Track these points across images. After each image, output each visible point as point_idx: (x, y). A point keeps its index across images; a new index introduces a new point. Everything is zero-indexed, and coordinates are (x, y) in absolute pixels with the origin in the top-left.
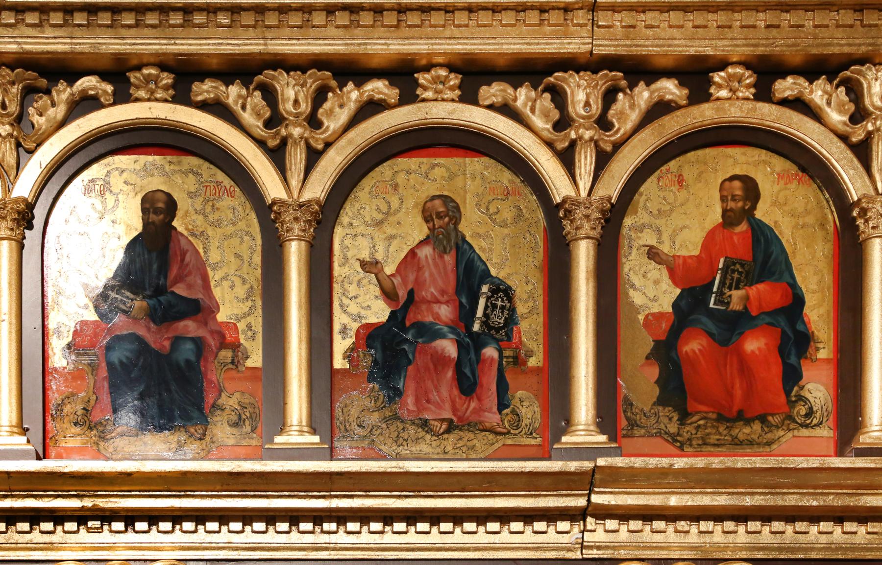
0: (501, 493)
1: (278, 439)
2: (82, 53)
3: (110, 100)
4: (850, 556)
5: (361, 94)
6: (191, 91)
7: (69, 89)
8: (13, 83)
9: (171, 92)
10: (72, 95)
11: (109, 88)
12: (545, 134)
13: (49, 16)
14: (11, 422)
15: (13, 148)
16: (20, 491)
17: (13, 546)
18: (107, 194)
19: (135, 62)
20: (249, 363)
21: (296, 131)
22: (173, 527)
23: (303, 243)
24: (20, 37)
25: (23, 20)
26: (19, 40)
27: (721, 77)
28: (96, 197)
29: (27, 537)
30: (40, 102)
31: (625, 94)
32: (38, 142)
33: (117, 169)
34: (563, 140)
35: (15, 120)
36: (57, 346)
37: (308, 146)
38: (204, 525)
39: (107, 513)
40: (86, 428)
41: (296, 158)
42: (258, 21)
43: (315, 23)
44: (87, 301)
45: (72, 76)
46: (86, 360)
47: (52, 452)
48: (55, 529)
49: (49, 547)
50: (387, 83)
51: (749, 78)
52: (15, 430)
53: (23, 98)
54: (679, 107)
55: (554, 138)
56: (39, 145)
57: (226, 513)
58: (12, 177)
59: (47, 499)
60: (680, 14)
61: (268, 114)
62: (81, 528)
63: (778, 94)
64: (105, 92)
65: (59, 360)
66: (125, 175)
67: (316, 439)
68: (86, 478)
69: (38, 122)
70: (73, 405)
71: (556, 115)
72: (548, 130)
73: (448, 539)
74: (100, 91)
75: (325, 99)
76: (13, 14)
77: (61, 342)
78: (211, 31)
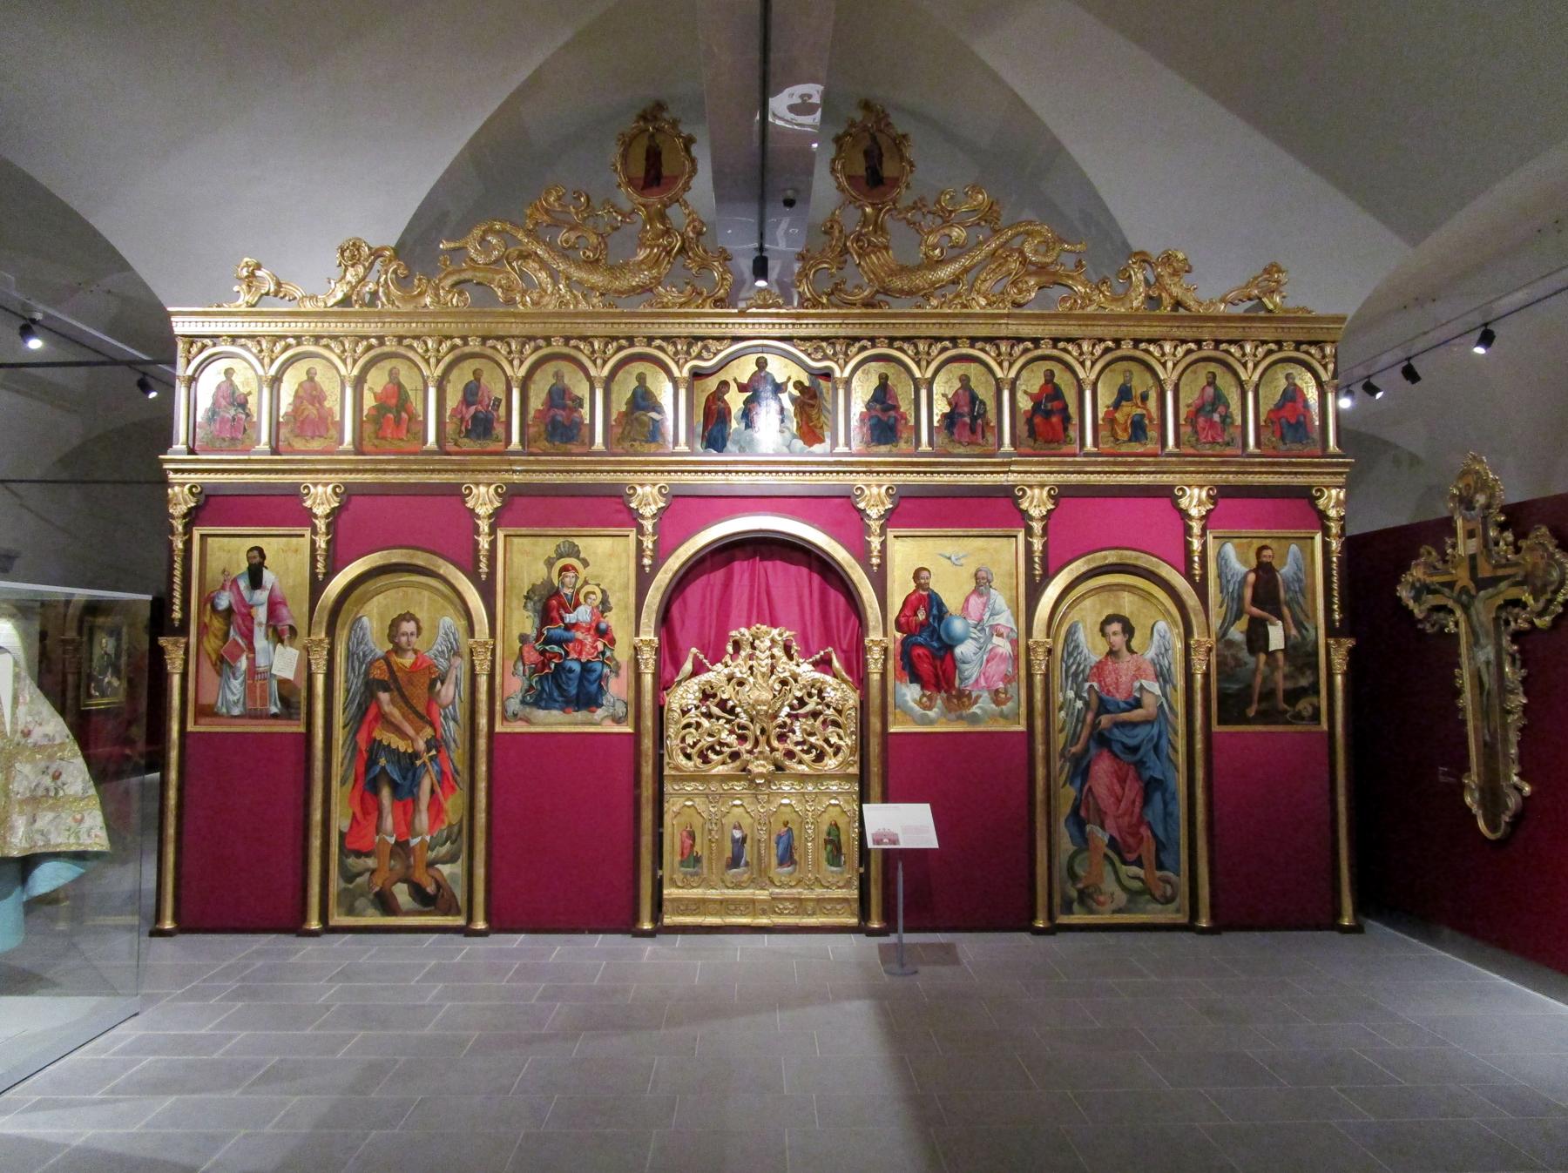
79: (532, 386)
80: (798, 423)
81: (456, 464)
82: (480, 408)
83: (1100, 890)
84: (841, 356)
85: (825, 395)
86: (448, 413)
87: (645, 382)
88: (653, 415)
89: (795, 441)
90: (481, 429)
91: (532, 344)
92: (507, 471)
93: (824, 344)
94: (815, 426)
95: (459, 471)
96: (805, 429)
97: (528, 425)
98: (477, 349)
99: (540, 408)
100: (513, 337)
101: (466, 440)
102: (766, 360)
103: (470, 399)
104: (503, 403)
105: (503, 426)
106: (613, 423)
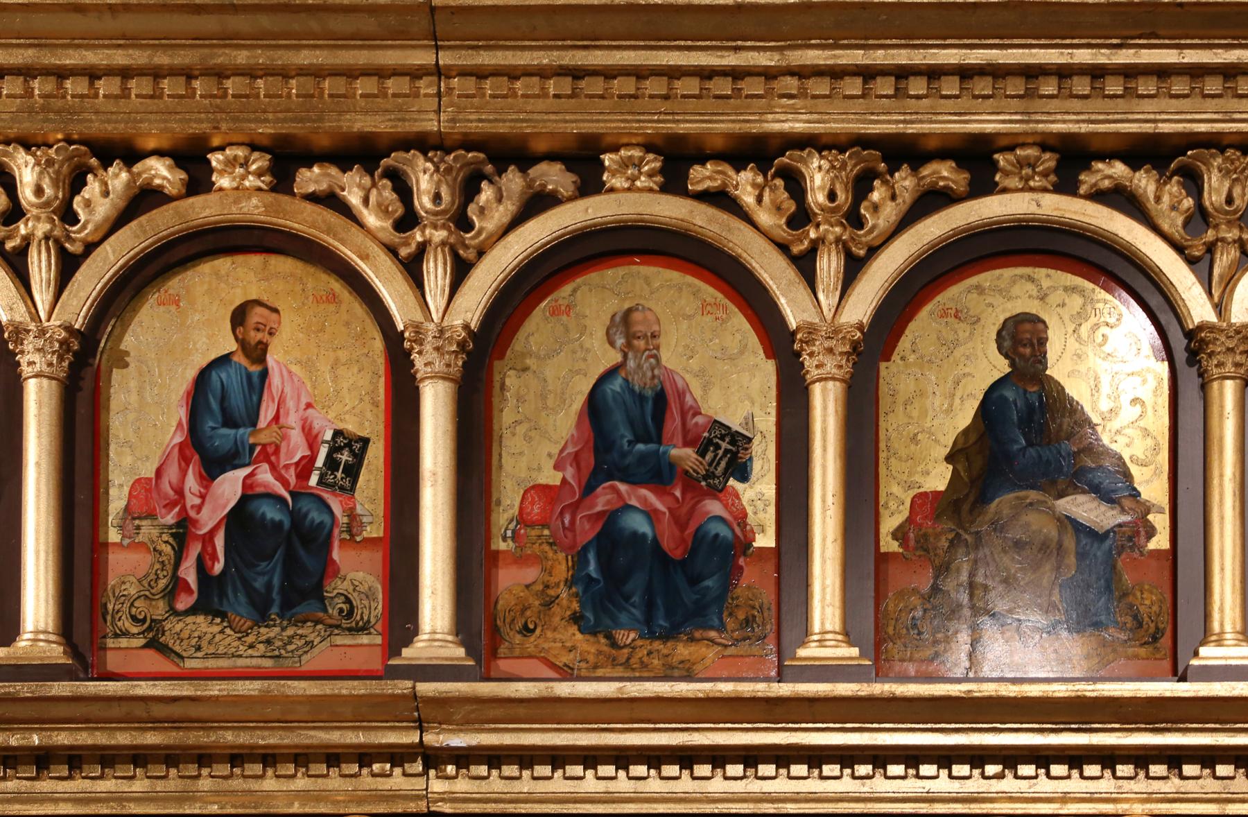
0: (810, 725)
4: (490, 808)
5: (134, 177)
6: (687, 178)
9: (659, 179)
12: (382, 236)
14: (1234, 628)
19: (1004, 142)
20: (1152, 545)
21: (439, 235)
27: (1007, 161)
31: (491, 182)
34: (407, 244)
37: (62, 251)
38: (338, 766)
41: (829, 265)
42: (1194, 88)
43: (1141, 90)
48: (874, 774)
50: (954, 165)
51: (653, 162)
52: (1241, 637)
54: (169, 199)
55: (397, 240)
56: (481, 253)
60: (342, 81)
61: (400, 212)
63: (692, 184)
67: (855, 651)
71: (791, 206)
72: (780, 226)
73: (542, 787)
75: (478, 191)
79: (511, 380)
81: (156, 723)
82: (265, 476)
86: (117, 501)
87: (1040, 358)
90: (268, 576)
91: (513, 181)
92: (397, 756)
95: (171, 758)
97: (494, 558)
98: (254, 209)
99: (552, 477)
100: (423, 144)
101: (201, 622)
103: (224, 437)
104: (376, 455)
105: (376, 558)
106: (889, 545)
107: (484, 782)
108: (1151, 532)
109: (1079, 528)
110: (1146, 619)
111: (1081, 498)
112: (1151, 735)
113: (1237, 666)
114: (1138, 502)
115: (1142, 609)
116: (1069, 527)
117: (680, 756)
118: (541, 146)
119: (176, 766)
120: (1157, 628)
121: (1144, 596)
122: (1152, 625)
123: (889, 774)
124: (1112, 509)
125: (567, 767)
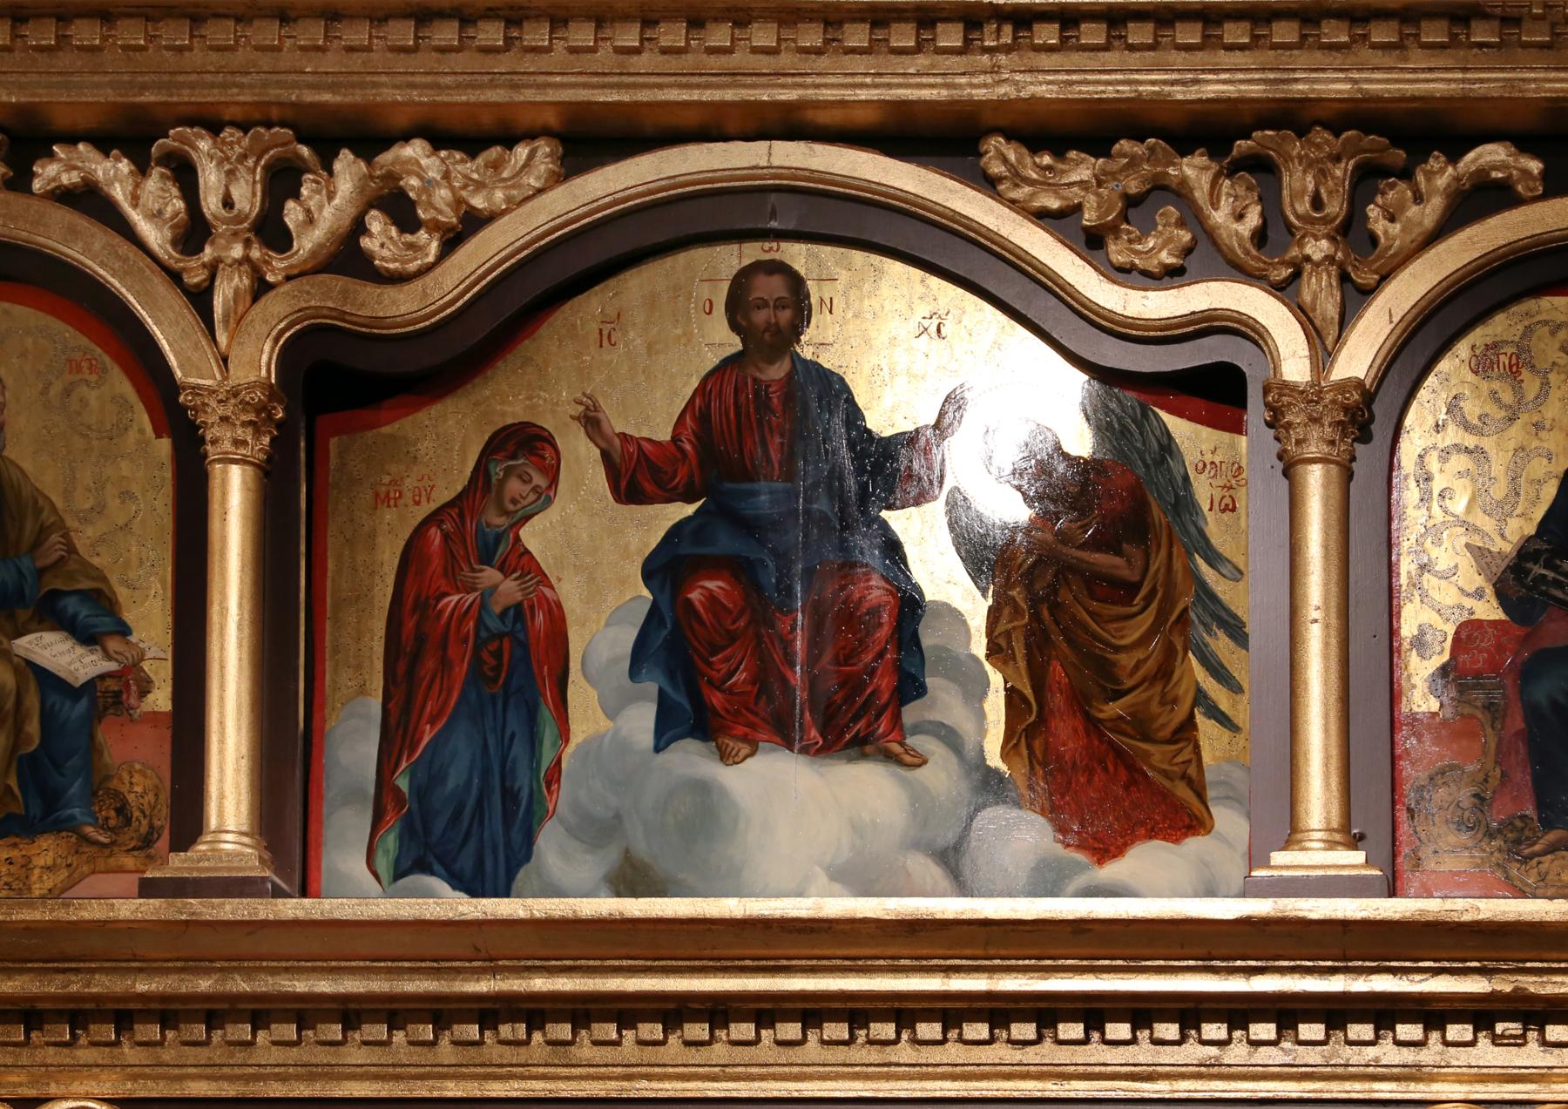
1: (1278, 858)
2: (1486, 99)
3: (1535, 189)
7: (1450, 169)
8: (1337, 159)
10: (1457, 179)
11: (1535, 166)
13: (1419, 28)
15: (1334, 284)
16: (1364, 960)
17: (1340, 1070)
18: (1525, 374)
22: (898, 1033)
23: (248, 468)
24: (1358, 69)
25: (1365, 37)
26: (1356, 76)
28: (1500, 377)
29: (1370, 1053)
30: (1391, 194)
32: (1384, 272)
33: (1546, 323)
35: (1337, 230)
36: (1420, 671)
39: (1539, 1007)
40: (1480, 836)
43: (1228, 39)
44: (1479, 581)
45: (1455, 147)
46: (1479, 697)
47: (1412, 880)
48: (1426, 1037)
49: (1414, 1073)
52: (1337, 837)
53: (1354, 186)
56: (1385, 278)
57: (1289, 1006)
58: (1329, 341)
59: (1418, 977)
62: (1481, 1035)
64: (1526, 173)
65: (1421, 699)
66: (1562, 335)
67: (1358, 857)
68: (812, 930)
69: (1386, 232)
70: (1453, 787)
74: (1515, 172)
76: (1345, 25)
77: (1426, 663)
78: (1111, 58)
80: (1012, 695)
83: (1008, 545)
84: (1318, 248)
85: (1215, 528)
88: (607, 740)
89: (995, 817)
93: (1194, 170)
94: (1141, 726)
96: (1066, 734)
102: (796, 283)
107: (523, 1050)
108: (145, 688)
109: (47, 680)
110: (137, 814)
111: (49, 637)
112: (1091, 976)
113: (1350, 877)
114: (128, 642)
115: (131, 798)
116: (31, 676)
117: (1230, 1010)
118: (401, 121)
119: (176, 1028)
120: (151, 826)
121: (134, 780)
122: (145, 822)
123: (1109, 1036)
124: (92, 652)
125: (1156, 1025)
